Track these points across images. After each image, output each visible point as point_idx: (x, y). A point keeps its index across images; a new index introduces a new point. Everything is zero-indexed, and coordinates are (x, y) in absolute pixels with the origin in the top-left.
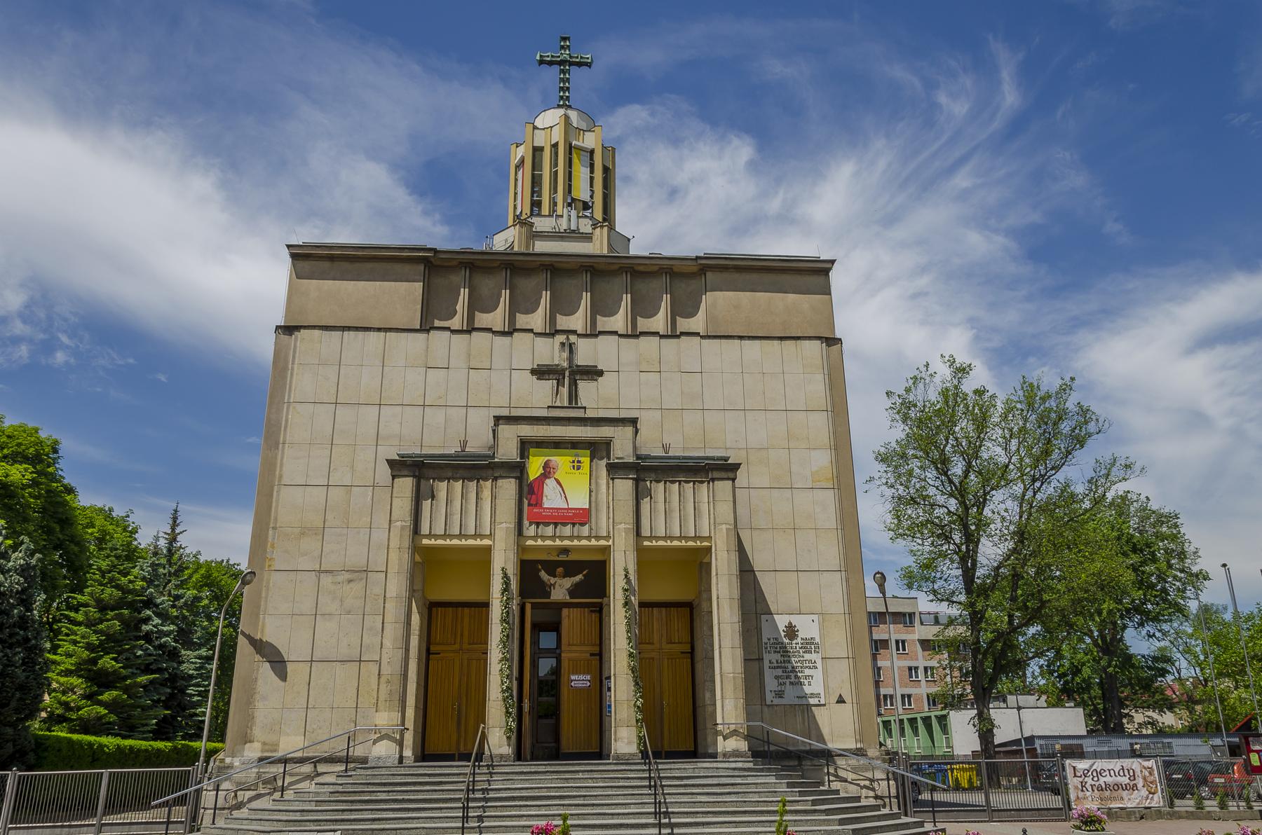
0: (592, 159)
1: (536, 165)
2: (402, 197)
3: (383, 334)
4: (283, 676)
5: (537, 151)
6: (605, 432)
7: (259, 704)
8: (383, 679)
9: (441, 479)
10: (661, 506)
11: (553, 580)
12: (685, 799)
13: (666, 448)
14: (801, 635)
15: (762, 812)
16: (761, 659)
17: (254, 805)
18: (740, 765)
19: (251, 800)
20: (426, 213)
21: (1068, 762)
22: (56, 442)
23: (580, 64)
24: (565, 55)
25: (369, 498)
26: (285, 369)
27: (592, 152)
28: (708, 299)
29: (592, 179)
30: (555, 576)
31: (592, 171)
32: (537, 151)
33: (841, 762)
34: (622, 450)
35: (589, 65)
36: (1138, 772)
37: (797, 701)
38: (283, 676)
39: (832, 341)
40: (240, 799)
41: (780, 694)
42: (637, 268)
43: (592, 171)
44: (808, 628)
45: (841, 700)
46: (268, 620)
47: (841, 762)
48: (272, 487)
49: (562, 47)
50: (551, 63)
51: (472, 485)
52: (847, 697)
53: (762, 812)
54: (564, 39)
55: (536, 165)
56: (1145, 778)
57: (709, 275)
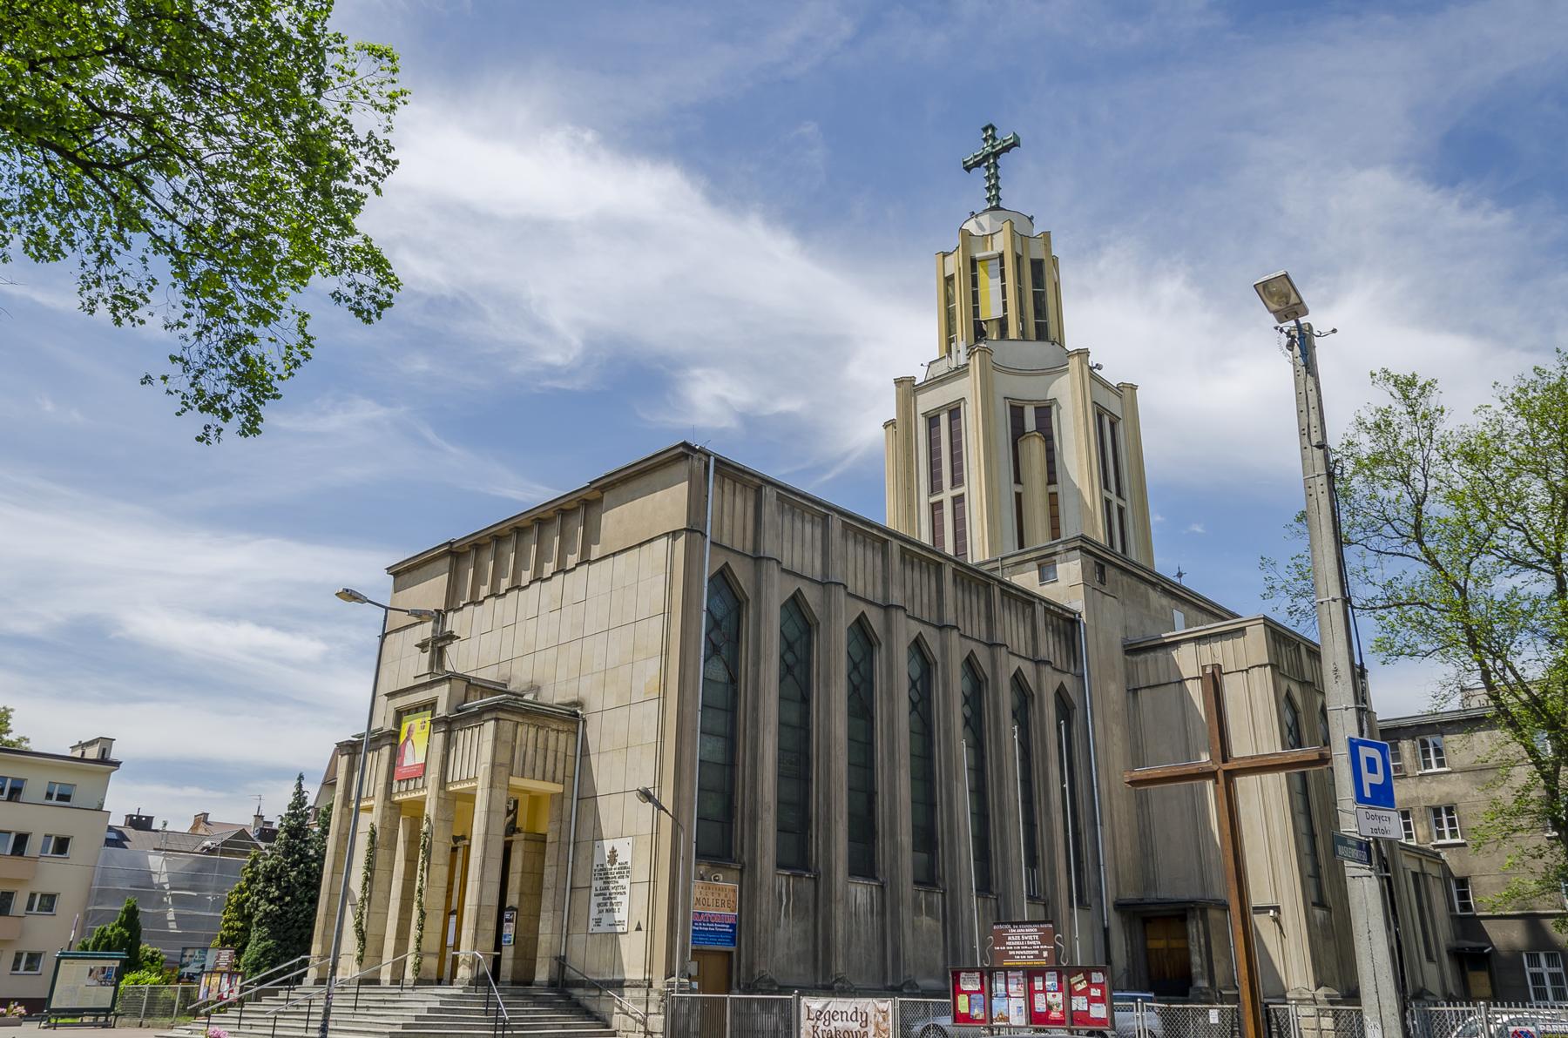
0: (1002, 264)
2: (1423, 197)
12: (370, 1019)
13: (535, 688)
14: (619, 860)
20: (1467, 206)
21: (804, 1000)
22: (106, 743)
23: (1006, 149)
29: (1004, 287)
31: (1003, 280)
33: (627, 992)
35: (1015, 144)
36: (871, 1018)
37: (609, 929)
41: (598, 922)
42: (566, 507)
43: (1003, 280)
44: (624, 856)
45: (639, 929)
47: (627, 992)
52: (644, 927)
56: (877, 1025)
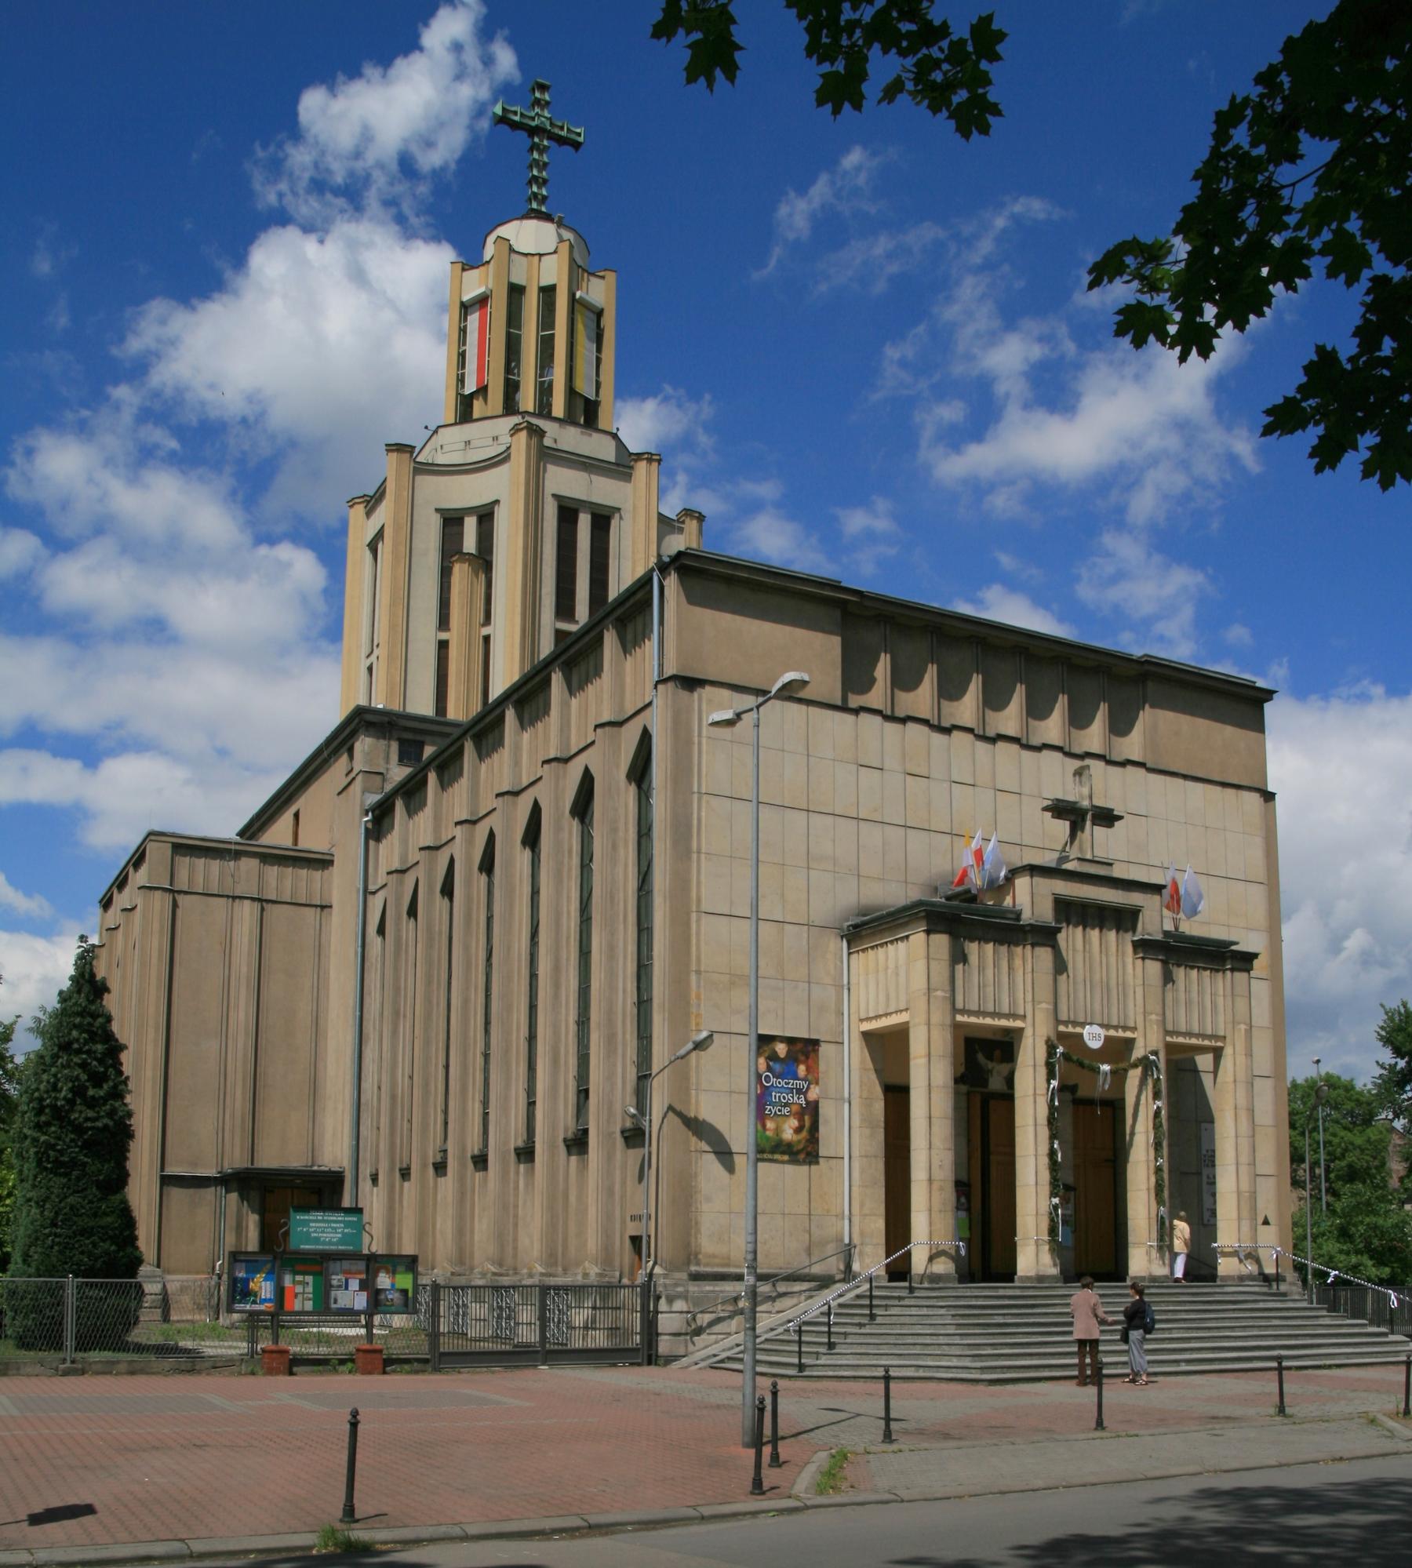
1: (514, 318)
3: (804, 707)
4: (730, 1168)
5: (516, 292)
6: (1135, 898)
7: (705, 1207)
8: (935, 1186)
9: (972, 940)
10: (1182, 996)
11: (990, 1065)
15: (1296, 1336)
16: (1199, 1174)
17: (717, 1328)
18: (1257, 1289)
19: (711, 1324)
23: (562, 141)
24: (542, 117)
25: (805, 943)
26: (689, 742)
27: (599, 314)
28: (1147, 717)
29: (599, 361)
30: (992, 1060)
31: (599, 350)
32: (516, 292)
34: (1155, 920)
38: (730, 1168)
39: (1269, 797)
40: (699, 1323)
43: (599, 350)
45: (1266, 1222)
46: (703, 1097)
48: (688, 914)
49: (537, 102)
50: (515, 126)
51: (1004, 949)
53: (1296, 1336)
54: (543, 88)
55: (514, 318)
57: (1150, 685)
